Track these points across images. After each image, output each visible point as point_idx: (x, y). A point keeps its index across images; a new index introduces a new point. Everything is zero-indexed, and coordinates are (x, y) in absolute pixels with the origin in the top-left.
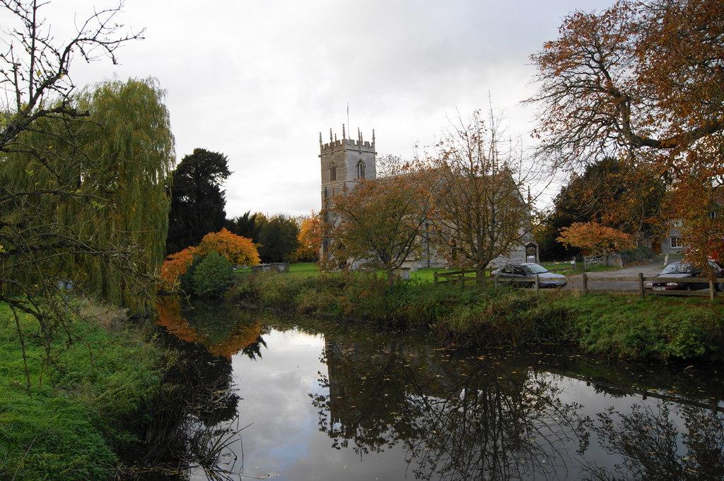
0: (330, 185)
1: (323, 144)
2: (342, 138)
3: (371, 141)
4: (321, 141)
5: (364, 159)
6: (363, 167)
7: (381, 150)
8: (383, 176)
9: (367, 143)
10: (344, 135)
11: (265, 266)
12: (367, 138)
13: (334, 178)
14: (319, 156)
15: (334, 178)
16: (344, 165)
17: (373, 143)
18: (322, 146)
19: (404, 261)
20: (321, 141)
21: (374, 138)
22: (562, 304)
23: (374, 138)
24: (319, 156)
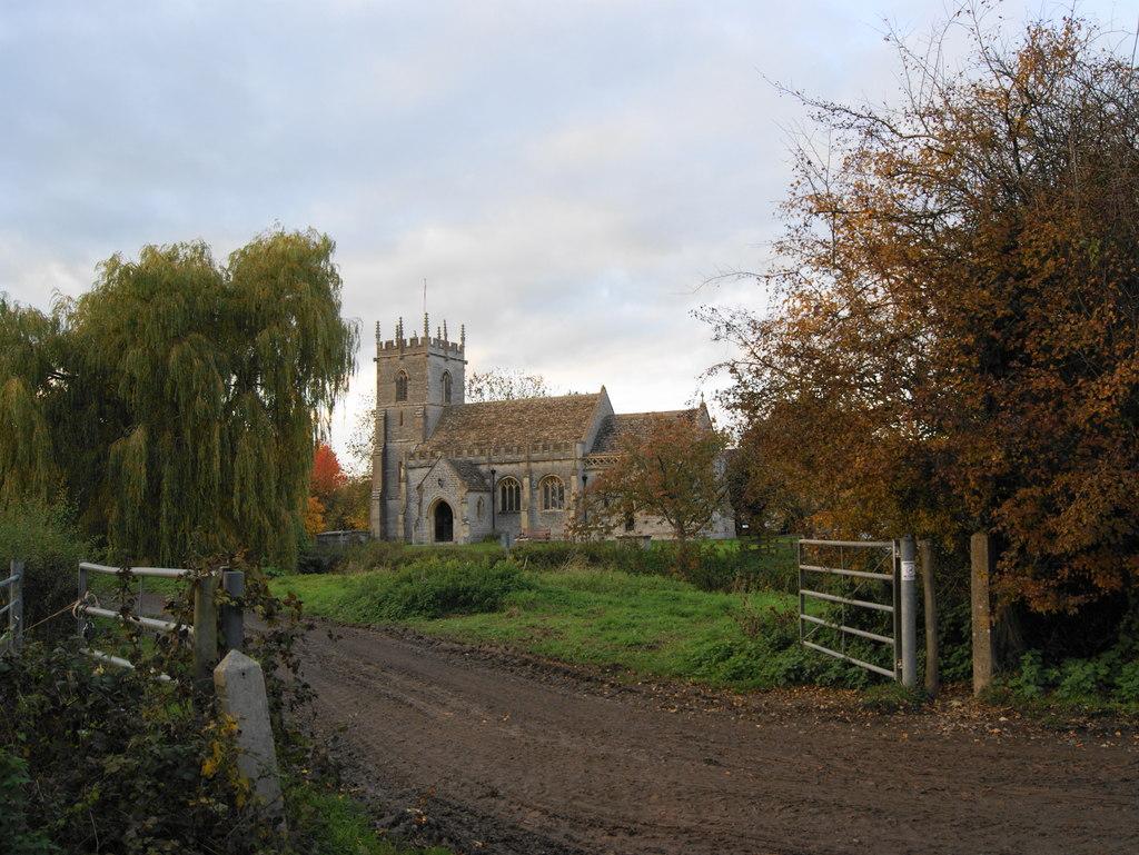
0: (394, 408)
1: (384, 340)
2: (423, 335)
3: (459, 343)
4: (378, 336)
5: (451, 370)
6: (451, 383)
7: (477, 360)
8: (67, 333)
9: (454, 345)
10: (427, 330)
11: (654, 587)
12: (454, 338)
13: (402, 395)
14: (375, 360)
15: (402, 395)
16: (424, 377)
17: (462, 347)
18: (379, 344)
19: (368, 533)
20: (378, 336)
21: (463, 339)
22: (711, 596)
23: (463, 339)
24: (375, 360)
